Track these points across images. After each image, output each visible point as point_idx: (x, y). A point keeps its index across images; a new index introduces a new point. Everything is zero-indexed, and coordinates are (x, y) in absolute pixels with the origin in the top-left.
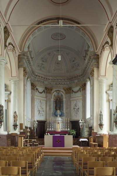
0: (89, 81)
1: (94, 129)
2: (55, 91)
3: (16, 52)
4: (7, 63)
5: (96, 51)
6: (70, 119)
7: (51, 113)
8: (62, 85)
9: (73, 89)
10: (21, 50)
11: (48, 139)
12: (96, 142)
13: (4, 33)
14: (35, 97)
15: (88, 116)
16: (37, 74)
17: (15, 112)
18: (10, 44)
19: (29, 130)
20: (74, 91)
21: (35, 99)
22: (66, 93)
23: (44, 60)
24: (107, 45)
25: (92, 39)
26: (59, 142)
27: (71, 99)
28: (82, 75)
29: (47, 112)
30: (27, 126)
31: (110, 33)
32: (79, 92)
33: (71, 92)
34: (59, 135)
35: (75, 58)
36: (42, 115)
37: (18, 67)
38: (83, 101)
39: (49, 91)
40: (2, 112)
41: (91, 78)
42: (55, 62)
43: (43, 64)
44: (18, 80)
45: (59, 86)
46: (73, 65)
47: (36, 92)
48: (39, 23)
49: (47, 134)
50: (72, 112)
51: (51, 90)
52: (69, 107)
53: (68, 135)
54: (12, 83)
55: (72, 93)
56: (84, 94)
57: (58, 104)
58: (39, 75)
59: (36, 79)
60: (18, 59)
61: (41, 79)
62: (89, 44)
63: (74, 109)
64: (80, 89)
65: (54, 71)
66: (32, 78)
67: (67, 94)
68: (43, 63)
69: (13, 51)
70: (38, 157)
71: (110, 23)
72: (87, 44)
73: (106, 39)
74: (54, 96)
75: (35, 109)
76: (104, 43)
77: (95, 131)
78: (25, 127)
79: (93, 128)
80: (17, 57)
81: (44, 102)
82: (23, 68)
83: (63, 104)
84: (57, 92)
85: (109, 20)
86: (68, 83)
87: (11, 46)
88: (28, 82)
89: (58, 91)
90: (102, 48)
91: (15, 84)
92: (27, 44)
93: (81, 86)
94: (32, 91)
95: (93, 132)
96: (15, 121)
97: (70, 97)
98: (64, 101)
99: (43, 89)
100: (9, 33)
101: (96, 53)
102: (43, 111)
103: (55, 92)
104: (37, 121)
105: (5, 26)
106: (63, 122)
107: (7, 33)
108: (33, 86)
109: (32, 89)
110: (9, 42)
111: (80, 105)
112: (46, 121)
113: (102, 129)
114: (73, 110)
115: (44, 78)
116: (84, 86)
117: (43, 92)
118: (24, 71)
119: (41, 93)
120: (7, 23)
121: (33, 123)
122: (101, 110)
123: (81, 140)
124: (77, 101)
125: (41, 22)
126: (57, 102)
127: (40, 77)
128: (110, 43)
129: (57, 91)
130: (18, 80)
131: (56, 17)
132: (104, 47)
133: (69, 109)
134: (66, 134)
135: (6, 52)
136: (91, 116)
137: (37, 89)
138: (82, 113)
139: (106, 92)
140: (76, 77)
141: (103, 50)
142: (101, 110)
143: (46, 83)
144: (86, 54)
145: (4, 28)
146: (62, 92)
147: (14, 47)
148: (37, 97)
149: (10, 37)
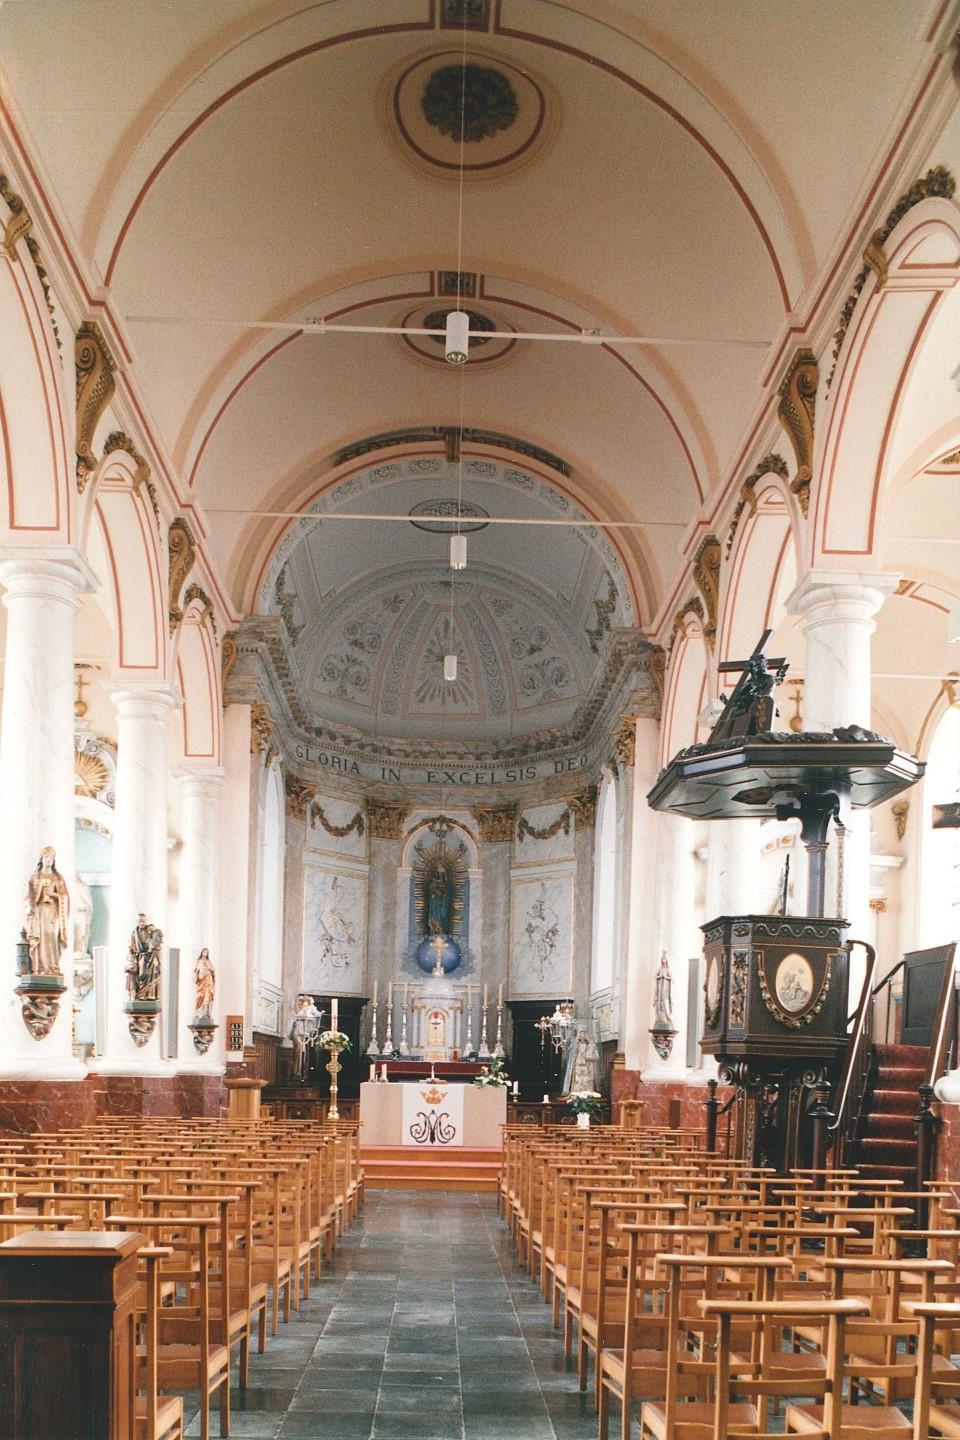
0: (613, 782)
1: (623, 1055)
2: (425, 822)
3: (214, 627)
5: (645, 630)
6: (507, 986)
9: (526, 814)
10: (239, 610)
13: (170, 550)
14: (307, 857)
16: (317, 723)
17: (204, 956)
18: (116, 441)
21: (307, 871)
22: (490, 837)
24: (771, 478)
25: (628, 552)
27: (513, 873)
28: (577, 739)
29: (372, 947)
32: (561, 831)
33: (517, 830)
36: (343, 963)
37: (221, 704)
38: (579, 885)
39: (385, 824)
40: (156, 963)
41: (620, 768)
42: (430, 651)
43: (354, 662)
44: (166, 693)
45: (445, 790)
46: (531, 671)
47: (313, 825)
48: (343, 456)
49: (809, 1018)
50: (517, 950)
51: (402, 815)
52: (499, 920)
55: (521, 839)
56: (589, 848)
57: (439, 898)
58: (331, 726)
59: (315, 753)
61: (342, 751)
62: (615, 577)
63: (530, 929)
64: (565, 816)
65: (422, 701)
66: (293, 745)
67: (489, 840)
69: (136, 488)
70: (315, 1223)
72: (608, 573)
74: (419, 849)
75: (304, 926)
76: (758, 460)
77: (631, 1064)
78: (254, 1033)
79: (620, 1051)
80: (220, 648)
81: (359, 887)
82: (247, 708)
84: (431, 829)
85: (788, 309)
86: (500, 775)
87: (197, 603)
88: (271, 774)
89: (442, 820)
91: (204, 795)
92: (275, 566)
93: (570, 798)
94: (287, 821)
95: (618, 1071)
96: (200, 1002)
97: (511, 864)
98: (472, 885)
100: (109, 368)
101: (650, 640)
102: (350, 940)
103: (425, 829)
105: (85, 324)
107: (185, 552)
108: (297, 795)
109: (287, 814)
111: (563, 908)
113: (665, 1057)
114: (526, 939)
115: (362, 747)
116: (592, 796)
117: (350, 828)
118: (255, 722)
119: (340, 832)
120: (102, 304)
122: (664, 953)
124: (548, 884)
125: (356, 450)
126: (433, 885)
127: (339, 741)
129: (434, 820)
130: (222, 777)
131: (438, 425)
132: (758, 488)
133: (499, 933)
135: (90, 497)
136: (616, 979)
137: (317, 811)
139: (696, 854)
140: (547, 745)
142: (664, 953)
143: (372, 771)
144: (604, 622)
145: (171, 528)
146: (464, 827)
147: (140, 462)
148: (315, 858)
149: (116, 395)
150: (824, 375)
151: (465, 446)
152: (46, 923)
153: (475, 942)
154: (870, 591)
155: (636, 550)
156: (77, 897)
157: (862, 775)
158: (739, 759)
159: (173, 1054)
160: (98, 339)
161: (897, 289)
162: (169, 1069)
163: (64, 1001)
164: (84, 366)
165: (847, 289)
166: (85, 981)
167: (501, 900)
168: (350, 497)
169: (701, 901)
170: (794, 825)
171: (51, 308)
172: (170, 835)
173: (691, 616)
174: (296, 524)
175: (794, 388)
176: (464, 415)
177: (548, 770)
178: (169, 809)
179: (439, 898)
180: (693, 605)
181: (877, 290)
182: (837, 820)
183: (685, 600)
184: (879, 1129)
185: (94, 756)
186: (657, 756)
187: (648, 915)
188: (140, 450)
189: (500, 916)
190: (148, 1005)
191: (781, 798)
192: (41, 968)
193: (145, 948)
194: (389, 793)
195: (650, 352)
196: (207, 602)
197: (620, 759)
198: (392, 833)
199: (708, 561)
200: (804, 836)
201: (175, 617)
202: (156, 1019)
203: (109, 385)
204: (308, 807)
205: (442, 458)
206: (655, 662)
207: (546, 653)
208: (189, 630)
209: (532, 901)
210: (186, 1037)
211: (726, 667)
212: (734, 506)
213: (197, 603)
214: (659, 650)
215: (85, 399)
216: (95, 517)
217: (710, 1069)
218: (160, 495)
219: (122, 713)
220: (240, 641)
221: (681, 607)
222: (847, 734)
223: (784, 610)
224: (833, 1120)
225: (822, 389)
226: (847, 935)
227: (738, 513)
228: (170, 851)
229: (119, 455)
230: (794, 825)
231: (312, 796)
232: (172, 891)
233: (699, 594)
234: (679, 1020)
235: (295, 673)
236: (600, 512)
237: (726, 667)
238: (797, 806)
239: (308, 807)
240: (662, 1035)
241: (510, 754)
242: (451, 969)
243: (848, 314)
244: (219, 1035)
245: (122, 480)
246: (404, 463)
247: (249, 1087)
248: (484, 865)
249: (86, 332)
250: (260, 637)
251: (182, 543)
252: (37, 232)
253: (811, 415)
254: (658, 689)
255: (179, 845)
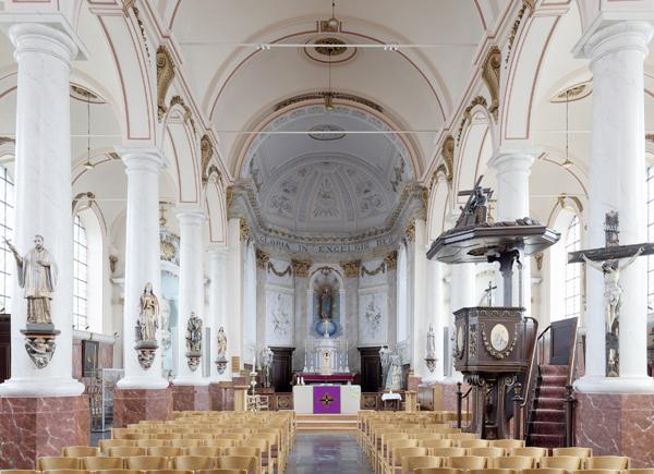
4: (83, 50)
7: (308, 326)
8: (336, 255)
10: (233, 176)
11: (303, 394)
12: (525, 364)
15: (402, 337)
16: (270, 226)
17: (221, 330)
18: (176, 100)
19: (254, 373)
20: (367, 268)
21: (267, 292)
22: (348, 275)
23: (290, 189)
24: (479, 107)
25: (409, 144)
26: (327, 402)
28: (387, 230)
30: (248, 363)
31: (448, 153)
34: (331, 385)
35: (370, 185)
41: (408, 243)
43: (285, 199)
45: (328, 255)
48: (279, 107)
49: (508, 354)
51: (308, 267)
52: (354, 312)
53: (352, 384)
54: (214, 256)
57: (326, 302)
59: (269, 240)
60: (228, 198)
63: (368, 315)
64: (383, 265)
66: (259, 236)
68: (286, 195)
71: (489, 38)
73: (477, 88)
74: (316, 281)
76: (472, 99)
77: (416, 374)
81: (290, 299)
83: (338, 302)
85: (485, 28)
86: (352, 248)
87: (214, 173)
89: (327, 268)
90: (463, 117)
91: (219, 259)
96: (220, 351)
99: (287, 264)
104: (273, 349)
106: (338, 352)
110: (175, 94)
111: (382, 305)
112: (294, 349)
113: (432, 371)
114: (366, 320)
115: (290, 236)
116: (395, 255)
119: (281, 275)
120: (168, 37)
121: (260, 355)
123: (385, 397)
128: (489, 103)
132: (472, 112)
133: (353, 318)
134: (345, 383)
136: (408, 337)
137: (271, 265)
138: (389, 328)
139: (444, 280)
140: (374, 234)
141: (527, 11)
143: (294, 247)
144: (399, 178)
147: (187, 109)
148: (271, 287)
149: (175, 78)
150: (504, 58)
151: (335, 100)
152: (149, 317)
153: (343, 321)
154: (529, 156)
155: (415, 147)
156: (162, 305)
157: (528, 241)
158: (472, 235)
159: (208, 375)
160: (166, 53)
161: (539, 16)
162: (206, 382)
163: (157, 352)
164: (160, 66)
165: (515, 17)
166: (167, 342)
167: (354, 303)
168: (284, 124)
169: (448, 301)
170: (496, 264)
171: (145, 39)
172: (205, 277)
173: (441, 172)
174: (258, 137)
175: (489, 65)
176: (336, 87)
177: (376, 246)
178: (204, 266)
179: (326, 302)
180: (442, 167)
181: (530, 16)
182: (518, 262)
183: (437, 166)
184: (544, 405)
185: (169, 243)
186: (426, 237)
187: (427, 310)
188: (187, 104)
189: (354, 310)
190: (196, 353)
191: (491, 253)
192: (147, 338)
193: (194, 328)
194: (301, 257)
195: (417, 51)
196: (219, 173)
197: (408, 236)
198: (304, 274)
199: (448, 147)
200: (501, 269)
201: (205, 179)
202: (200, 359)
203: (172, 74)
204: (266, 264)
205: (324, 106)
206: (423, 194)
207: (373, 193)
208: (211, 185)
209: (368, 303)
210: (214, 367)
211: (462, 194)
212: (460, 121)
213: (214, 173)
214: (425, 189)
215: (161, 81)
216: (167, 135)
217: (459, 377)
218: (196, 124)
219: (181, 225)
220: (235, 191)
221: (436, 169)
222: (522, 222)
223: (486, 167)
224: (522, 402)
225: (503, 64)
226: (525, 314)
227: (462, 125)
228: (205, 285)
229: (177, 106)
230: (496, 264)
231: (268, 258)
232: (206, 302)
233: (444, 162)
234: (439, 355)
235: (259, 204)
236: (396, 127)
237: (462, 194)
238: (498, 255)
239: (266, 264)
240: (430, 361)
241: (357, 238)
242: (332, 334)
243: (515, 28)
244: (229, 365)
245: (116, 3)
246: (306, 109)
247: (243, 389)
248: (346, 287)
249: (161, 50)
250: (243, 188)
251: (206, 146)
252: (193, 117)
253: (498, 77)
254: (425, 207)
255: (209, 282)
